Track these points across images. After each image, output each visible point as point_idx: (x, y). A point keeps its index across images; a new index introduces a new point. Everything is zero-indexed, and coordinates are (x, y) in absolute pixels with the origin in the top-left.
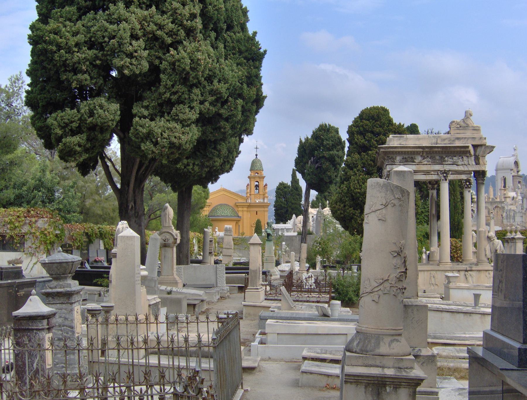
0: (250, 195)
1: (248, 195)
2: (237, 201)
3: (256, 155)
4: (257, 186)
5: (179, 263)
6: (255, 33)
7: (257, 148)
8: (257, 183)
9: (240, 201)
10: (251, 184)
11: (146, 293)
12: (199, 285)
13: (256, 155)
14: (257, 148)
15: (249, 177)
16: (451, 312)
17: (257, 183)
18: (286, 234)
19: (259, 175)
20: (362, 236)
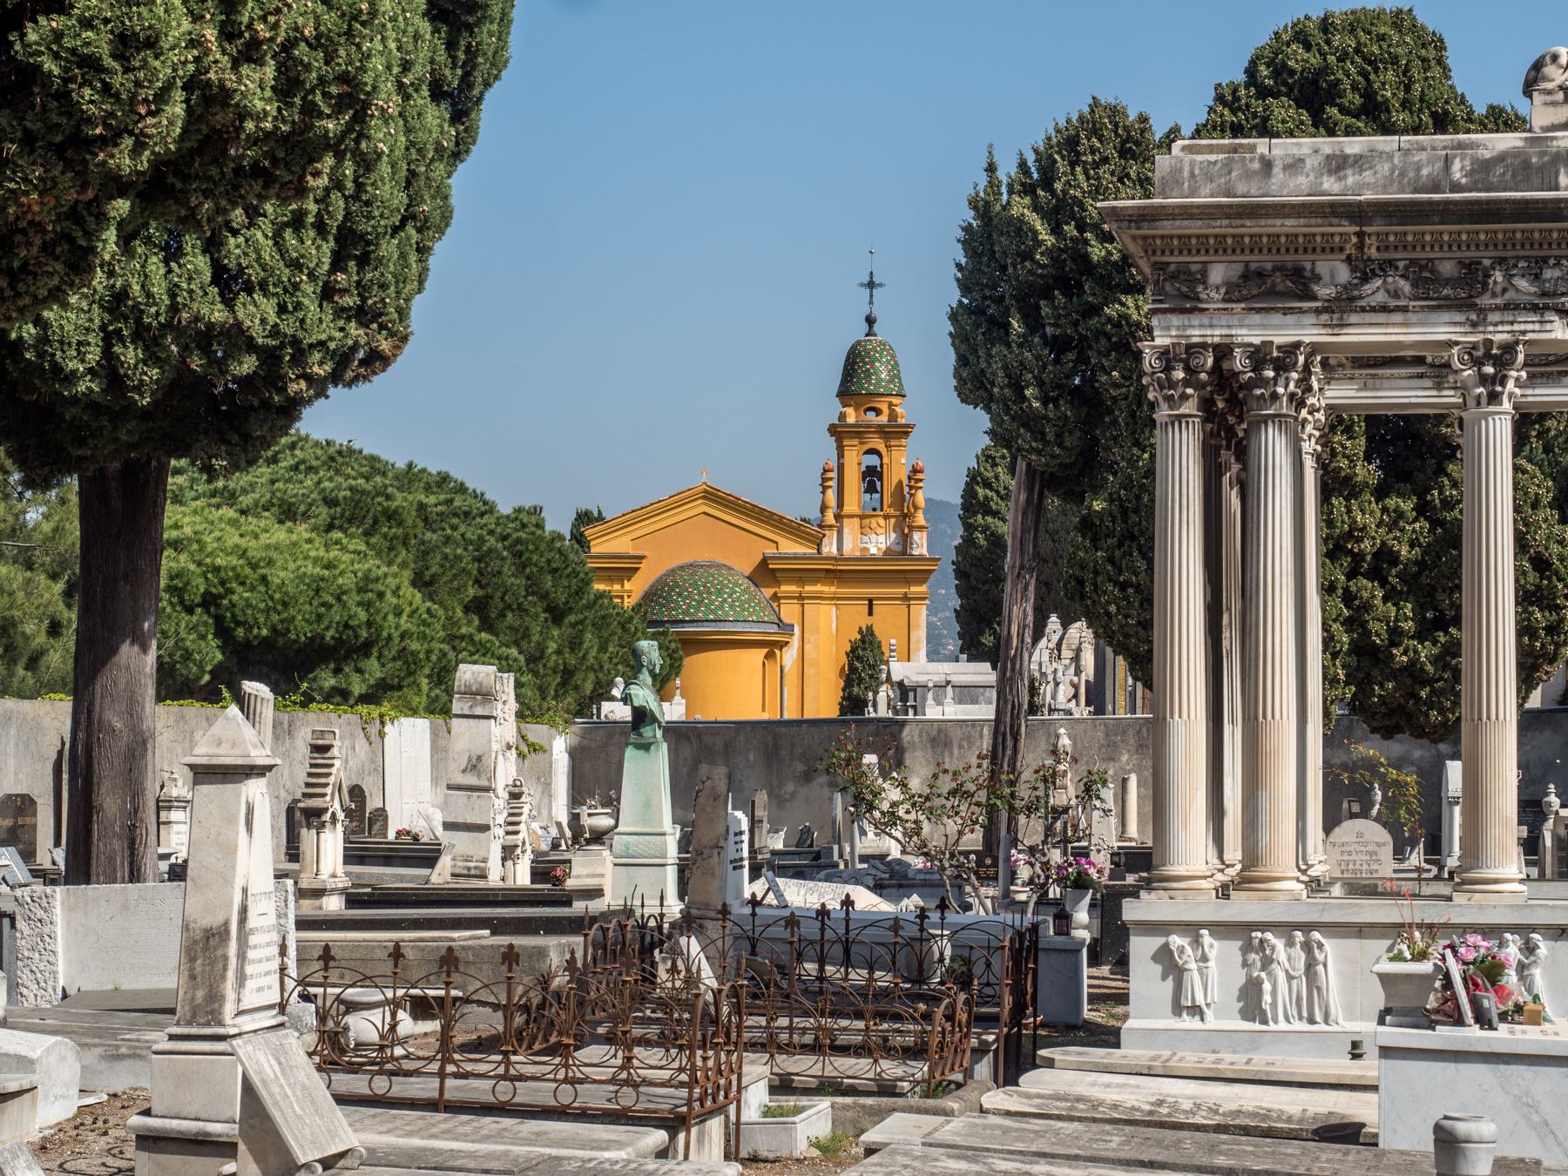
0: (838, 517)
1: (830, 518)
2: (770, 550)
3: (870, 321)
4: (872, 477)
5: (1117, 1045)
6: (1164, 978)
7: (871, 285)
8: (873, 460)
9: (790, 547)
10: (841, 468)
11: (1500, 1154)
12: (136, 994)
13: (870, 321)
14: (871, 285)
15: (833, 430)
16: (1065, 951)
17: (873, 460)
18: (1319, 221)
19: (883, 419)
20: (868, 888)
